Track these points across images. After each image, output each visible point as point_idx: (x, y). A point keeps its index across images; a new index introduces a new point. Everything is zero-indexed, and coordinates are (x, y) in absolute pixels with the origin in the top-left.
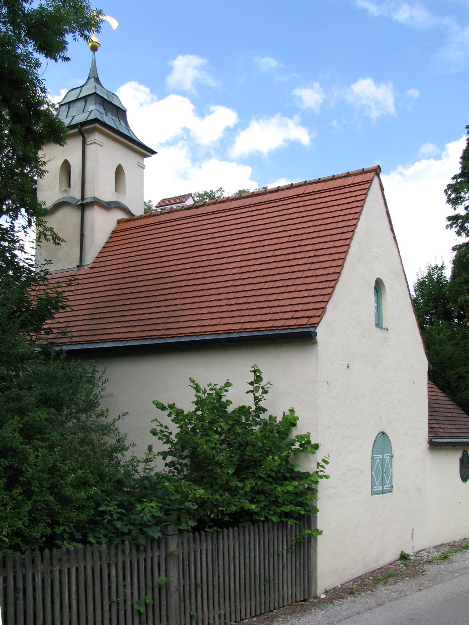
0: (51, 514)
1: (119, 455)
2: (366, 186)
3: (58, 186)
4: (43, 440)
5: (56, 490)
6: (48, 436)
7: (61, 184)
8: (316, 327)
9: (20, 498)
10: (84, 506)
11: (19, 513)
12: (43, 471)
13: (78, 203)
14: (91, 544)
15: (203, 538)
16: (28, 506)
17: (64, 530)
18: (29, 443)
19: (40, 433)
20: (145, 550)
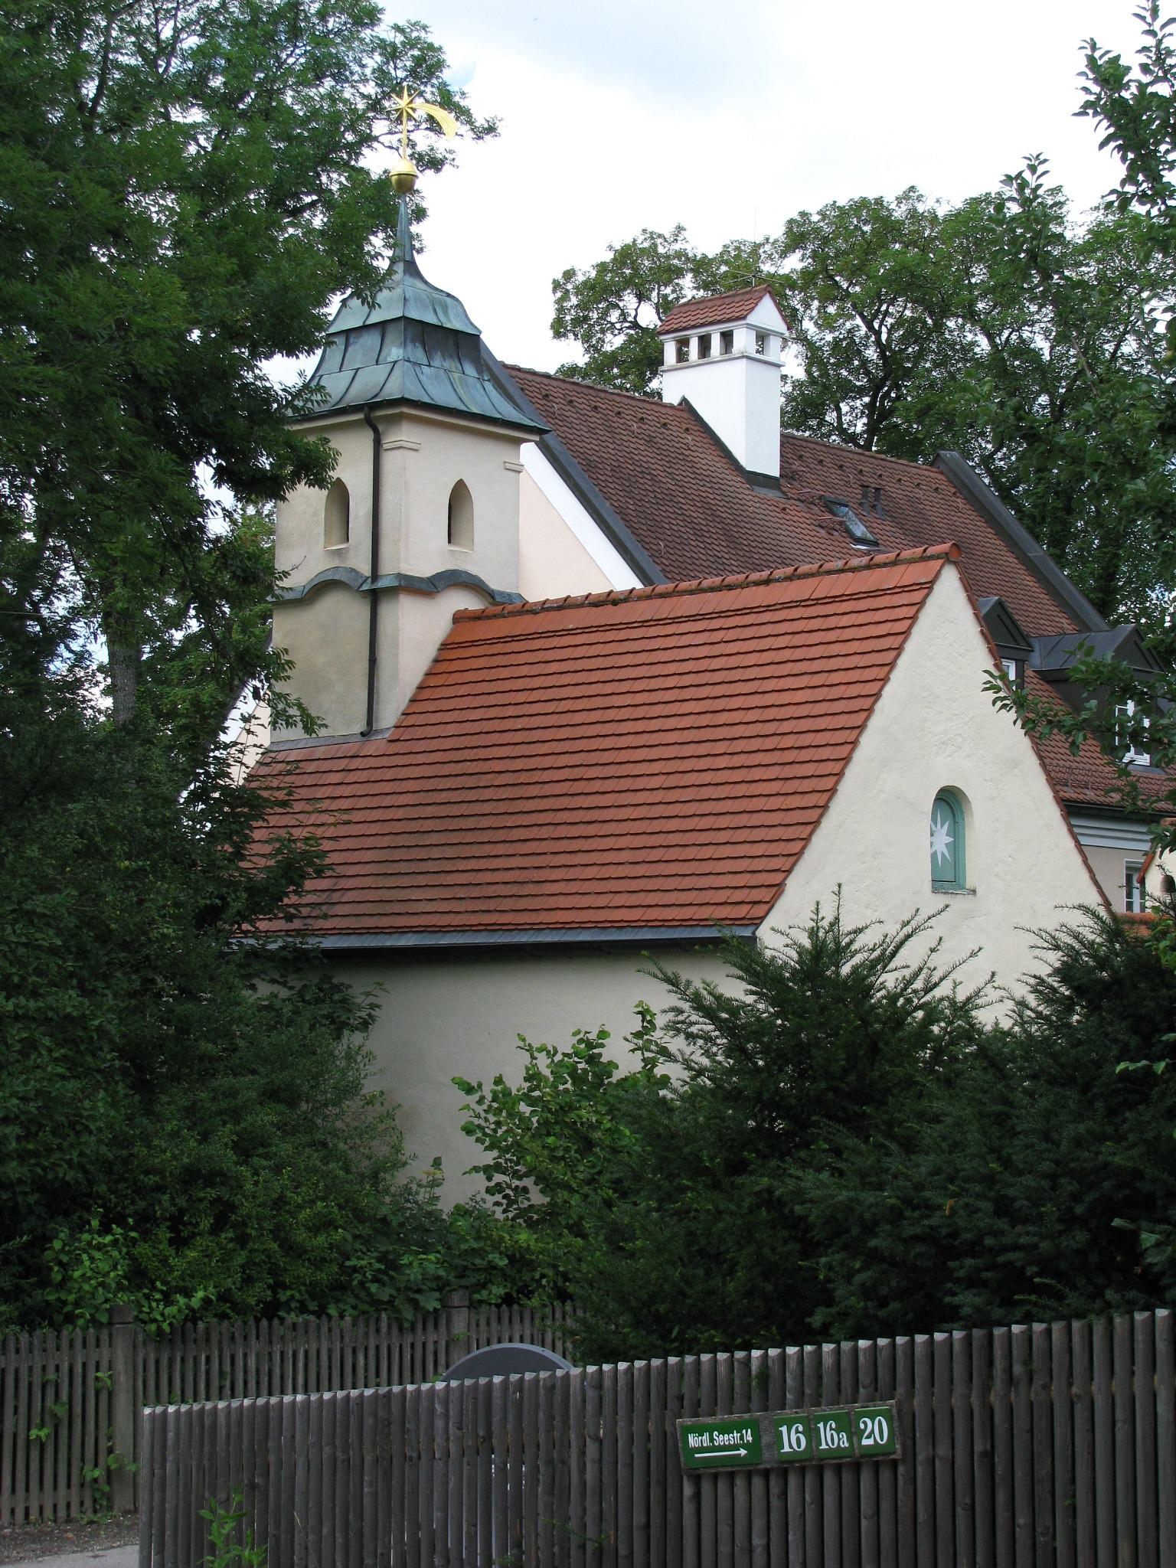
0: (274, 1271)
1: (388, 1177)
2: (917, 597)
3: (322, 538)
4: (266, 1156)
5: (282, 1234)
6: (274, 1149)
7: (327, 533)
8: (758, 925)
9: (231, 1245)
10: (323, 1260)
11: (228, 1269)
12: (263, 1205)
13: (365, 587)
14: (330, 1317)
15: (516, 1318)
16: (241, 1258)
17: (292, 1297)
18: (246, 1162)
19: (263, 1145)
20: (413, 1329)
